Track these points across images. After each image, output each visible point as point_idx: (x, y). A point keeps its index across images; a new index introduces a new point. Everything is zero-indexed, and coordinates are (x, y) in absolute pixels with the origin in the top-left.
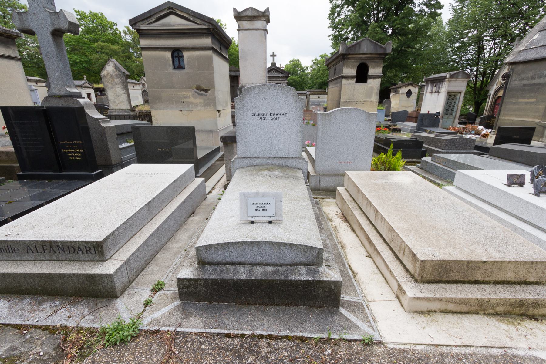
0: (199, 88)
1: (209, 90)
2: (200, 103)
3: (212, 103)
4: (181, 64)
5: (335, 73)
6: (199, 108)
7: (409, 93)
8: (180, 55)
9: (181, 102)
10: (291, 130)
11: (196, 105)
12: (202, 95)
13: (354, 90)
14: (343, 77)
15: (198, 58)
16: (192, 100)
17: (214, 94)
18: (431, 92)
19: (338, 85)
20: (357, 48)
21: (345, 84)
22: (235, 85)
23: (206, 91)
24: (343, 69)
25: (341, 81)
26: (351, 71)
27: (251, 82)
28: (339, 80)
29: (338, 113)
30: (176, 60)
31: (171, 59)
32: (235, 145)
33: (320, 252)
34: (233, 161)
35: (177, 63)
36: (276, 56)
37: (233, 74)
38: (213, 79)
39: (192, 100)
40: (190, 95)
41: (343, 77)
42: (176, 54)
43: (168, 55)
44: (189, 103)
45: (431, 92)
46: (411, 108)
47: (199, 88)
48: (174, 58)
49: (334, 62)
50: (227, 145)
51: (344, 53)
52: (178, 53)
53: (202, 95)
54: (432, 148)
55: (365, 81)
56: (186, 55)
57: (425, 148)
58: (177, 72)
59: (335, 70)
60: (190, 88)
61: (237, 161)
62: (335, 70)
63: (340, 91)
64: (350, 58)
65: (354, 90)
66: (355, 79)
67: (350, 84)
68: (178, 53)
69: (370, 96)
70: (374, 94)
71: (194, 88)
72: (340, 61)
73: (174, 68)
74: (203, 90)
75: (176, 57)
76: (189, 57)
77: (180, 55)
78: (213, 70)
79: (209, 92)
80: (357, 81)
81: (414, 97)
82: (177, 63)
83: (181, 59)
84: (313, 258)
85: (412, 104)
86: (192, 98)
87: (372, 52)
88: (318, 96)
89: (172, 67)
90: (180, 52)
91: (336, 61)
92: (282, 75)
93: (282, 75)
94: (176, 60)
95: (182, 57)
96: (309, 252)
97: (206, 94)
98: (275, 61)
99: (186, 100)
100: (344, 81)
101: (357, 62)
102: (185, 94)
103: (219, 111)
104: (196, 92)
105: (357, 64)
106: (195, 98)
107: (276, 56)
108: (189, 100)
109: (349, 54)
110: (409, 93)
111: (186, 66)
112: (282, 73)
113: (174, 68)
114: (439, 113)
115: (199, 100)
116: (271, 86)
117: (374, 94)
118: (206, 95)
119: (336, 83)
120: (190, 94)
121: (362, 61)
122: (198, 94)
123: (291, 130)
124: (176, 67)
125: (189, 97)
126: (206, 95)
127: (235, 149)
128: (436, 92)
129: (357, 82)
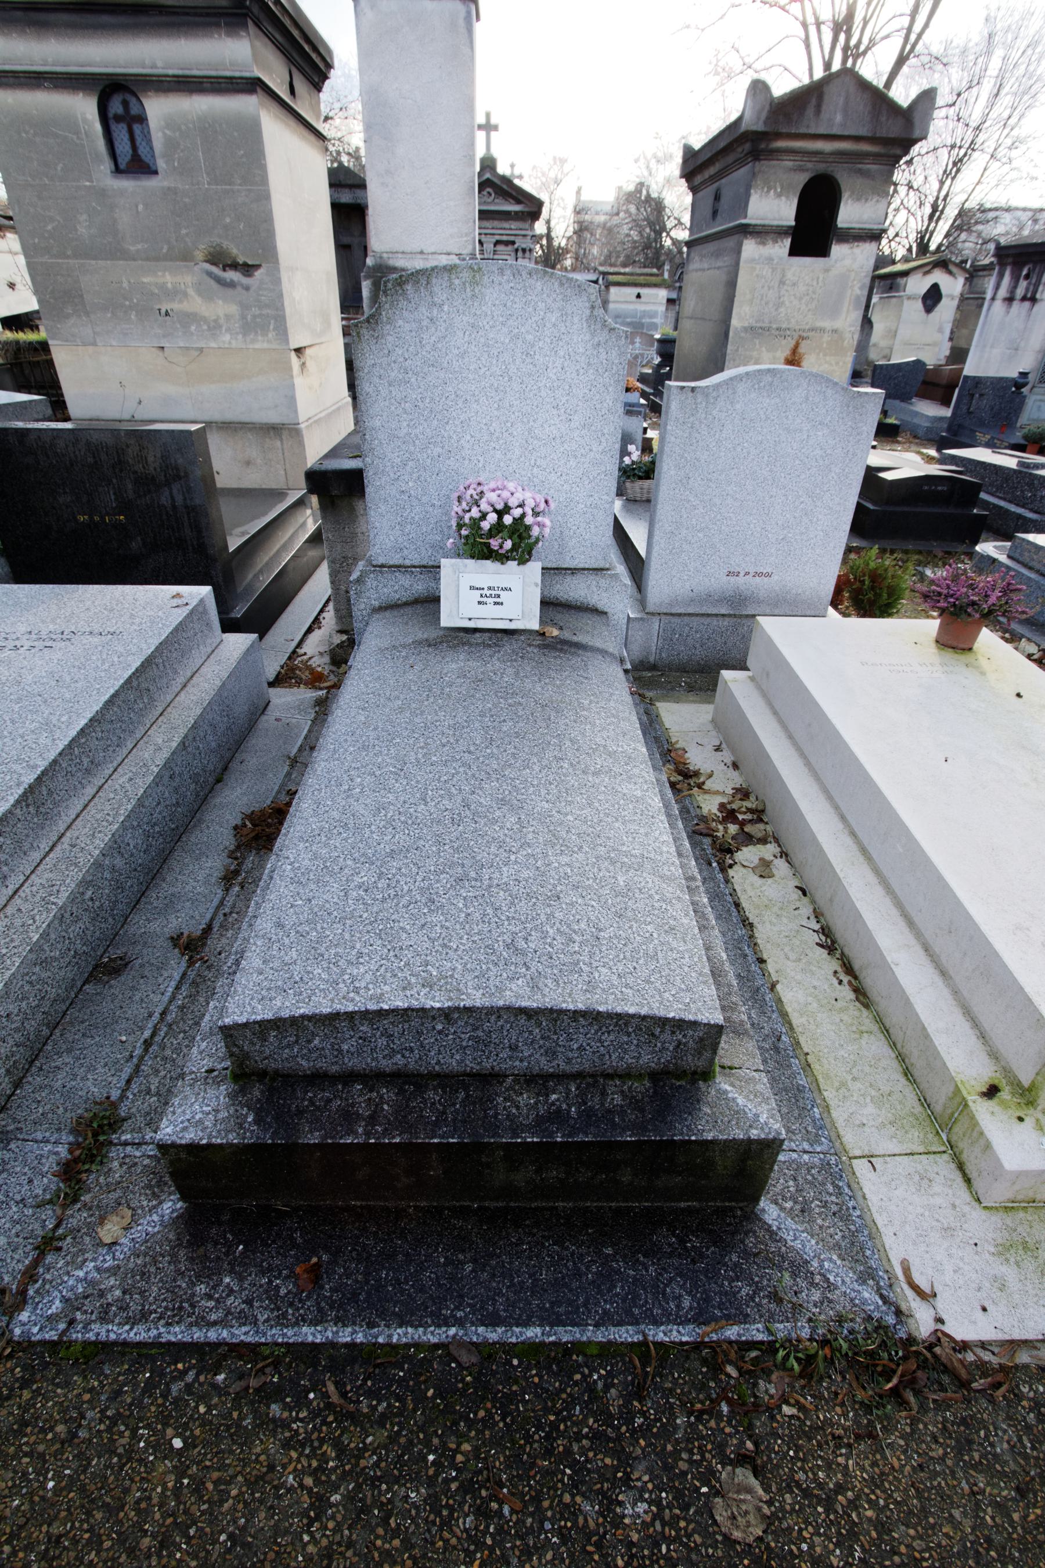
0: (221, 259)
1: (258, 267)
2: (228, 317)
3: (269, 318)
4: (142, 151)
5: (715, 213)
6: (227, 337)
7: (932, 297)
8: (134, 110)
9: (154, 312)
10: (573, 463)
11: (214, 327)
12: (232, 285)
13: (782, 282)
14: (746, 231)
15: (208, 129)
16: (196, 304)
17: (278, 281)
18: (1010, 300)
19: (726, 261)
20: (810, 112)
21: (753, 260)
22: (354, 241)
23: (248, 269)
24: (748, 196)
25: (740, 246)
26: (774, 206)
27: (416, 247)
28: (730, 242)
29: (741, 387)
30: (120, 133)
31: (98, 127)
32: (359, 505)
33: (710, 1036)
34: (358, 581)
35: (123, 147)
36: (496, 128)
37: (346, 197)
38: (267, 219)
39: (196, 304)
40: (187, 286)
41: (746, 231)
42: (116, 107)
43: (84, 108)
44: (189, 319)
45: (1010, 300)
46: (933, 353)
47: (221, 259)
48: (113, 126)
49: (712, 170)
50: (333, 503)
51: (760, 127)
52: (125, 104)
53: (232, 285)
54: (1002, 503)
55: (822, 251)
56: (158, 109)
57: (986, 505)
58: (127, 184)
59: (717, 197)
60: (186, 257)
61: (370, 582)
62: (717, 197)
63: (732, 284)
64: (778, 151)
65: (782, 282)
66: (788, 242)
67: (770, 259)
68: (125, 104)
69: (834, 311)
70: (846, 304)
71: (199, 255)
72: (739, 163)
73: (118, 170)
74: (234, 266)
75: (118, 119)
76: (170, 123)
77: (134, 110)
78: (264, 180)
79: (258, 274)
80: (795, 251)
81: (947, 310)
82: (123, 147)
83: (137, 128)
84: (678, 1060)
85: (937, 337)
86: (199, 300)
87: (863, 131)
88: (636, 291)
89: (107, 165)
90: (133, 101)
91: (730, 159)
92: (517, 208)
93: (517, 208)
94: (120, 133)
95: (142, 119)
96: (666, 1036)
97: (245, 280)
98: (495, 152)
99: (175, 306)
100: (750, 248)
101: (801, 169)
102: (169, 279)
103: (299, 351)
104: (210, 274)
105: (803, 178)
106: (207, 296)
107: (496, 128)
108: (185, 306)
109: (778, 136)
110: (932, 297)
111: (161, 164)
112: (519, 202)
113: (118, 170)
114: (1024, 375)
115: (222, 308)
116: (501, 271)
117: (846, 304)
118: (247, 288)
119: (717, 255)
120: (188, 279)
121: (821, 168)
122: (219, 281)
123: (573, 463)
124: (122, 166)
125: (185, 295)
126: (247, 288)
127: (362, 520)
128: (1024, 299)
129: (794, 252)
